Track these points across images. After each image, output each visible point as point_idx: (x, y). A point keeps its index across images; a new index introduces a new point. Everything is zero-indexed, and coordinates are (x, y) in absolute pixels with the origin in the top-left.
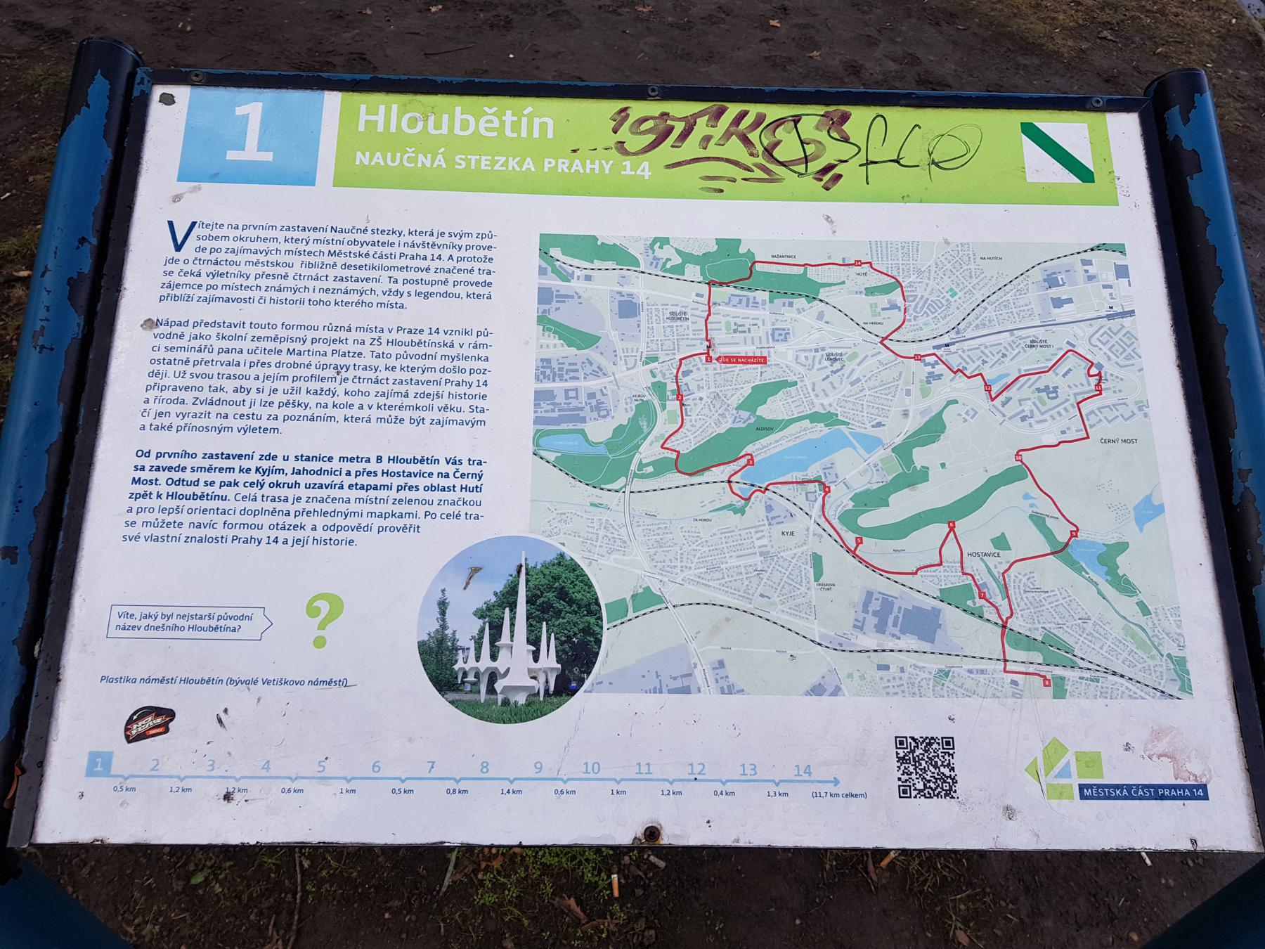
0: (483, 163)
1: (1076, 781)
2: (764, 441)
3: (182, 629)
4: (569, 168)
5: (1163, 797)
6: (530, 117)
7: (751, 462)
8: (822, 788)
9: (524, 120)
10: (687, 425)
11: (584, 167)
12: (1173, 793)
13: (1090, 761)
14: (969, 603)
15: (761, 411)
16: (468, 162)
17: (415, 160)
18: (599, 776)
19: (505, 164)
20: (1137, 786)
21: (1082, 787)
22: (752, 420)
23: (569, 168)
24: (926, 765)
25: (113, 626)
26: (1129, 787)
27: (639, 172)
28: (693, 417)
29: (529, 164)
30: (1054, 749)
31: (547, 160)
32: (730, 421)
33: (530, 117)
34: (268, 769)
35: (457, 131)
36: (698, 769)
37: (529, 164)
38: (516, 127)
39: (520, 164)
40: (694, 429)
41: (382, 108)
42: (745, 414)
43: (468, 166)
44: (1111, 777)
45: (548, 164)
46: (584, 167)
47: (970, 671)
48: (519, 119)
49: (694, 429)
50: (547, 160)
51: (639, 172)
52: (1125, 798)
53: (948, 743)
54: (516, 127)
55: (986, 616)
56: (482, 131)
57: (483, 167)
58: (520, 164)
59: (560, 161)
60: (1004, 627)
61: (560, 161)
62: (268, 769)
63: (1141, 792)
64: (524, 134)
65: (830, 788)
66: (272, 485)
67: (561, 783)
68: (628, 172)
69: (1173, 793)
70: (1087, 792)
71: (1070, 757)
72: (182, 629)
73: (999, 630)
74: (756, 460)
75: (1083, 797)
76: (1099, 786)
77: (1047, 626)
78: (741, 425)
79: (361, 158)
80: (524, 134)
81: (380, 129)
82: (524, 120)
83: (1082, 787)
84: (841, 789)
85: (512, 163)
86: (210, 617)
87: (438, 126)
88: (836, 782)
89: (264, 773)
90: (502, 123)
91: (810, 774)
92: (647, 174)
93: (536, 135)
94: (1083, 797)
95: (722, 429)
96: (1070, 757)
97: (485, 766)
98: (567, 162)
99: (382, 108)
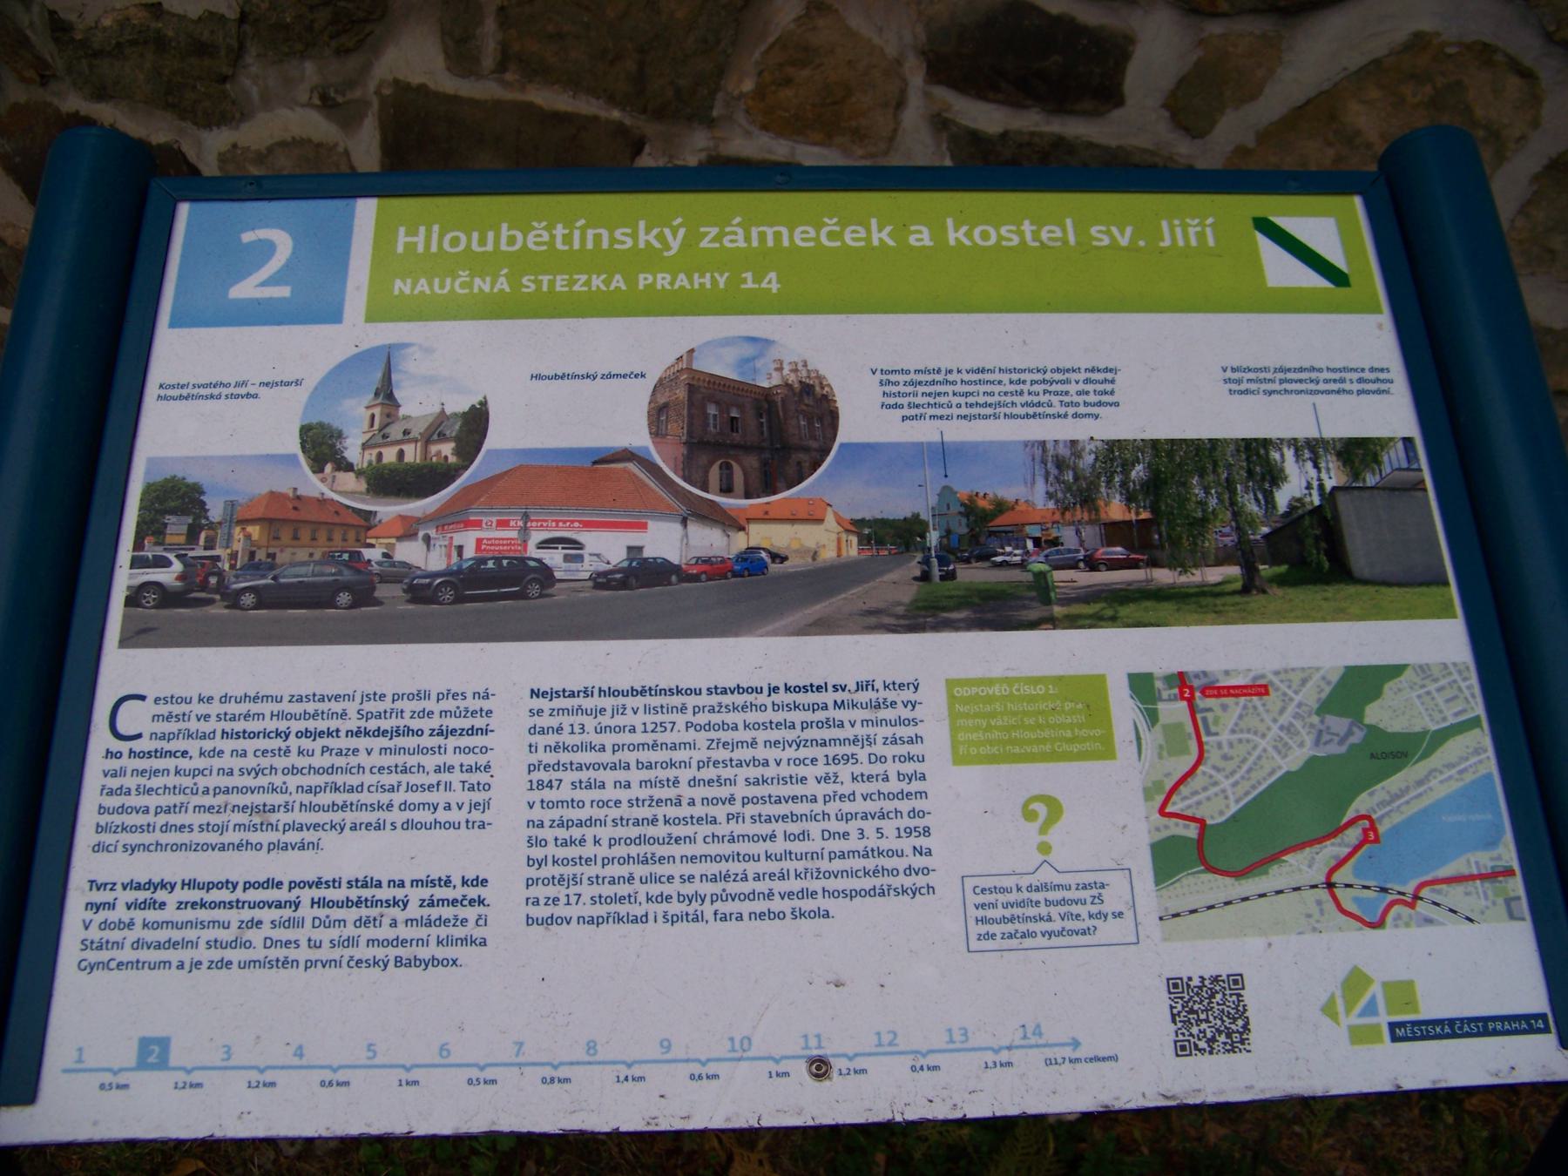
0: (558, 283)
1: (1383, 1019)
2: (1395, 782)
4: (672, 284)
5: (1495, 1033)
6: (583, 230)
7: (1371, 835)
8: (1058, 1053)
9: (577, 233)
10: (1213, 756)
11: (692, 284)
12: (1507, 1026)
13: (1402, 991)
15: (1374, 714)
16: (538, 283)
17: (470, 285)
19: (588, 283)
20: (1462, 1020)
21: (1393, 1026)
22: (1358, 736)
23: (672, 284)
24: (1209, 1012)
25: (973, 937)
26: (1451, 1022)
27: (764, 285)
28: (1225, 737)
29: (618, 282)
30: (1355, 981)
31: (641, 276)
32: (1309, 740)
33: (583, 230)
34: (301, 1056)
35: (504, 247)
36: (886, 1038)
37: (618, 282)
38: (568, 239)
39: (607, 282)
40: (1230, 766)
42: (1339, 724)
43: (539, 287)
44: (1429, 1010)
45: (644, 280)
46: (692, 284)
48: (571, 233)
49: (1230, 766)
50: (641, 276)
51: (764, 285)
52: (1447, 1036)
53: (1183, 1048)
54: (568, 239)
56: (531, 246)
57: (558, 289)
58: (607, 282)
59: (659, 276)
61: (659, 276)
62: (301, 1056)
63: (1466, 1029)
64: (576, 246)
65: (1068, 1052)
66: (299, 735)
67: (698, 1065)
68: (750, 285)
70: (1400, 1032)
71: (1376, 989)
74: (1382, 829)
75: (1395, 1039)
76: (1414, 1023)
78: (1334, 749)
79: (401, 286)
80: (576, 246)
81: (421, 249)
82: (577, 233)
83: (1393, 1026)
85: (597, 282)
87: (483, 242)
88: (1076, 1044)
89: (296, 1061)
90: (553, 237)
91: (1040, 1034)
92: (775, 287)
93: (590, 246)
94: (1395, 1039)
95: (1294, 760)
96: (1376, 989)
98: (668, 277)
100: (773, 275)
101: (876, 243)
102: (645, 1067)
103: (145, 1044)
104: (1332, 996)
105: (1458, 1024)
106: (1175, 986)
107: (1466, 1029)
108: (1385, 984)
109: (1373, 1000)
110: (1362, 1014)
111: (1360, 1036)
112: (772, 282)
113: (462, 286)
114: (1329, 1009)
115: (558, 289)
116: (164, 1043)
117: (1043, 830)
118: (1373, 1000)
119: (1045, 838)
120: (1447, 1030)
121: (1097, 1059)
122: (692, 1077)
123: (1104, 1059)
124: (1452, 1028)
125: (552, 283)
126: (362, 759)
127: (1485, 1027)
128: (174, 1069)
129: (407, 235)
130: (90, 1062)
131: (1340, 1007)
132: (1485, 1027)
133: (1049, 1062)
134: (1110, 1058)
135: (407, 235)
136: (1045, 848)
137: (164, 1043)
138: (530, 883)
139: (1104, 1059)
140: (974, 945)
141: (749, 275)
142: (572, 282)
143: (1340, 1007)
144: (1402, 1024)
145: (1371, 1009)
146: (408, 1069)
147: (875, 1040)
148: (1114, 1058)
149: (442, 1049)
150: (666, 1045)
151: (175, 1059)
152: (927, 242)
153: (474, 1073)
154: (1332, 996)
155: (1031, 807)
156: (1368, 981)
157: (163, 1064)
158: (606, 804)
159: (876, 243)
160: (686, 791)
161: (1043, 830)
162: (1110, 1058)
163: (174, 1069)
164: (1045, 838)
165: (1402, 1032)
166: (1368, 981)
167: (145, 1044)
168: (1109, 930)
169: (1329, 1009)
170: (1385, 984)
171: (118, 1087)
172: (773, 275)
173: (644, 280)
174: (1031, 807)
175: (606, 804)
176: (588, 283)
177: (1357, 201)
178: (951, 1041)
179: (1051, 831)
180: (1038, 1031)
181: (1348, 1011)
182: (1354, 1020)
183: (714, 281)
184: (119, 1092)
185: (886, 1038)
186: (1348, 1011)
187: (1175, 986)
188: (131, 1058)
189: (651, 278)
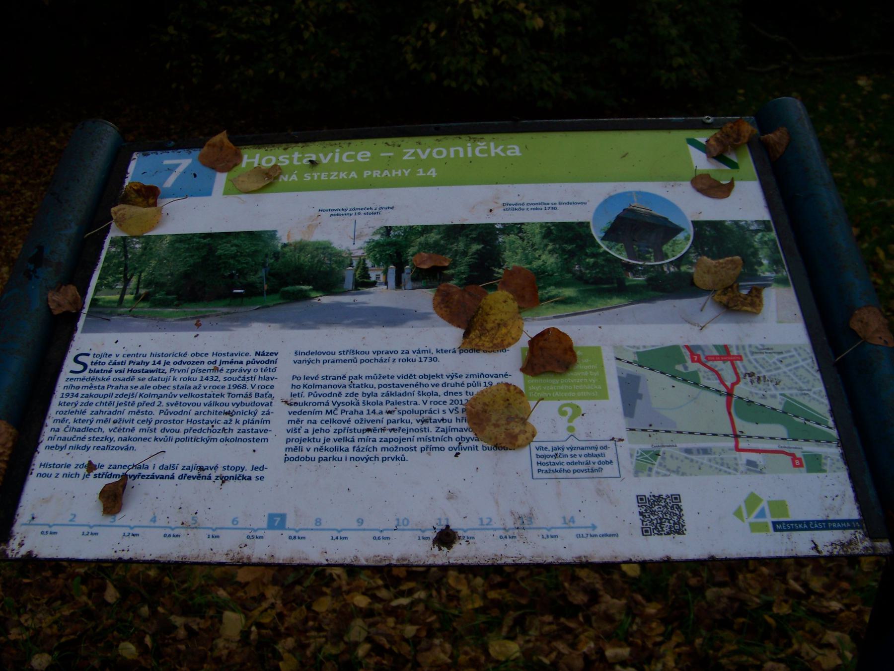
1: (769, 520)
3: (568, 471)
5: (832, 528)
8: (583, 531)
13: (779, 506)
14: (679, 368)
16: (313, 177)
18: (409, 527)
20: (813, 521)
21: (774, 523)
24: (662, 514)
25: (535, 471)
26: (808, 522)
29: (354, 175)
30: (752, 500)
34: (155, 521)
36: (486, 521)
37: (354, 175)
41: (258, 156)
44: (795, 515)
45: (366, 174)
46: (391, 174)
47: (688, 451)
52: (805, 530)
53: (647, 531)
55: (704, 382)
60: (729, 394)
68: (421, 174)
69: (839, 525)
71: (764, 504)
72: (568, 471)
73: (723, 399)
75: (776, 530)
76: (786, 522)
77: (787, 392)
83: (774, 523)
84: (599, 531)
86: (575, 471)
88: (594, 527)
89: (152, 524)
91: (574, 522)
94: (776, 530)
96: (764, 504)
97: (360, 521)
99: (258, 156)
100: (433, 170)
101: (493, 154)
102: (219, 531)
103: (271, 517)
104: (740, 508)
105: (811, 524)
106: (642, 499)
107: (816, 526)
108: (769, 503)
109: (763, 510)
110: (757, 517)
111: (754, 527)
112: (433, 173)
113: (481, 152)
114: (738, 513)
115: (322, 178)
116: (283, 517)
117: (571, 420)
118: (763, 510)
119: (571, 424)
120: (805, 526)
121: (606, 535)
122: (374, 538)
123: (610, 535)
124: (808, 525)
125: (319, 177)
126: (172, 383)
127: (827, 525)
128: (289, 529)
129: (248, 158)
130: (78, 521)
131: (745, 515)
132: (827, 525)
133: (578, 536)
134: (613, 535)
135: (248, 158)
136: (571, 429)
137: (283, 517)
138: (288, 441)
139: (610, 535)
140: (536, 475)
141: (421, 170)
142: (329, 176)
143: (745, 515)
144: (779, 523)
145: (762, 514)
146: (214, 530)
147: (479, 522)
148: (617, 535)
149: (233, 521)
150: (360, 521)
151: (289, 523)
152: (518, 154)
153: (335, 534)
154: (740, 508)
155: (564, 409)
156: (760, 500)
157: (282, 526)
158: (438, 403)
159: (493, 154)
160: (419, 399)
161: (571, 420)
162: (613, 535)
163: (289, 529)
164: (571, 424)
165: (778, 526)
166: (760, 500)
167: (271, 517)
168: (608, 470)
169: (738, 513)
170: (769, 503)
171: (51, 533)
172: (433, 170)
173: (366, 174)
174: (564, 409)
175: (438, 403)
176: (338, 176)
177: (113, 209)
178: (482, 524)
179: (575, 421)
180: (572, 520)
181: (749, 514)
182: (752, 519)
183: (403, 173)
184: (214, 540)
185: (486, 521)
186: (749, 514)
187: (642, 499)
188: (264, 525)
189: (370, 173)
